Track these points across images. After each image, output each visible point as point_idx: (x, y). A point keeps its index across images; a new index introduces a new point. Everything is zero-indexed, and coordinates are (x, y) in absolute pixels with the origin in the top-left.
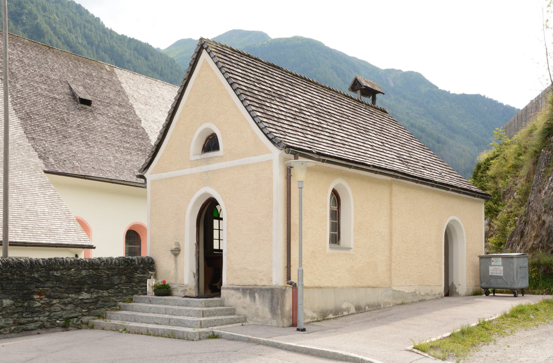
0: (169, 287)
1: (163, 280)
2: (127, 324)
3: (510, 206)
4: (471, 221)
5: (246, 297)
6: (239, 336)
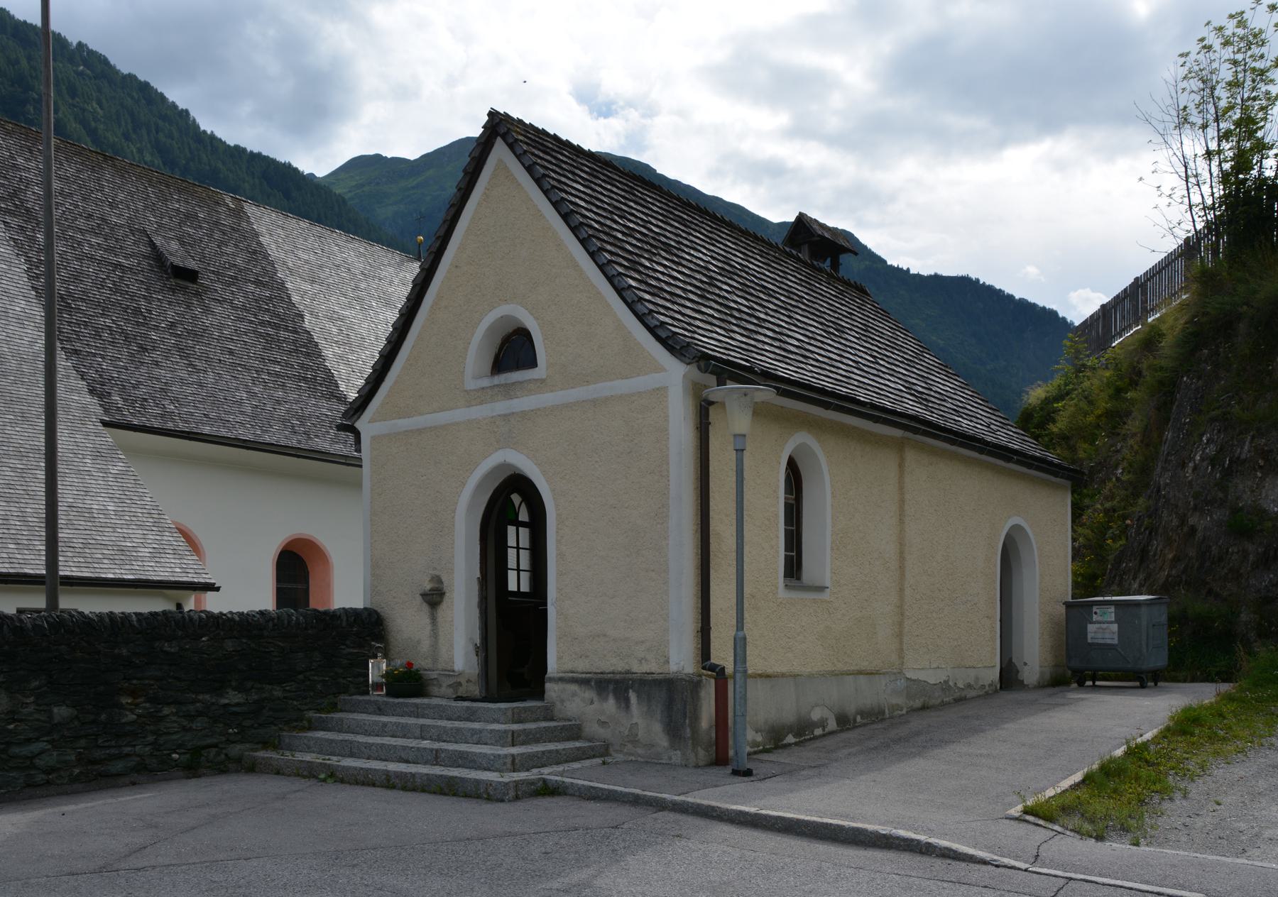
1: (405, 661)
2: (334, 760)
3: (1111, 497)
4: (1047, 525)
5: (606, 699)
6: (610, 791)
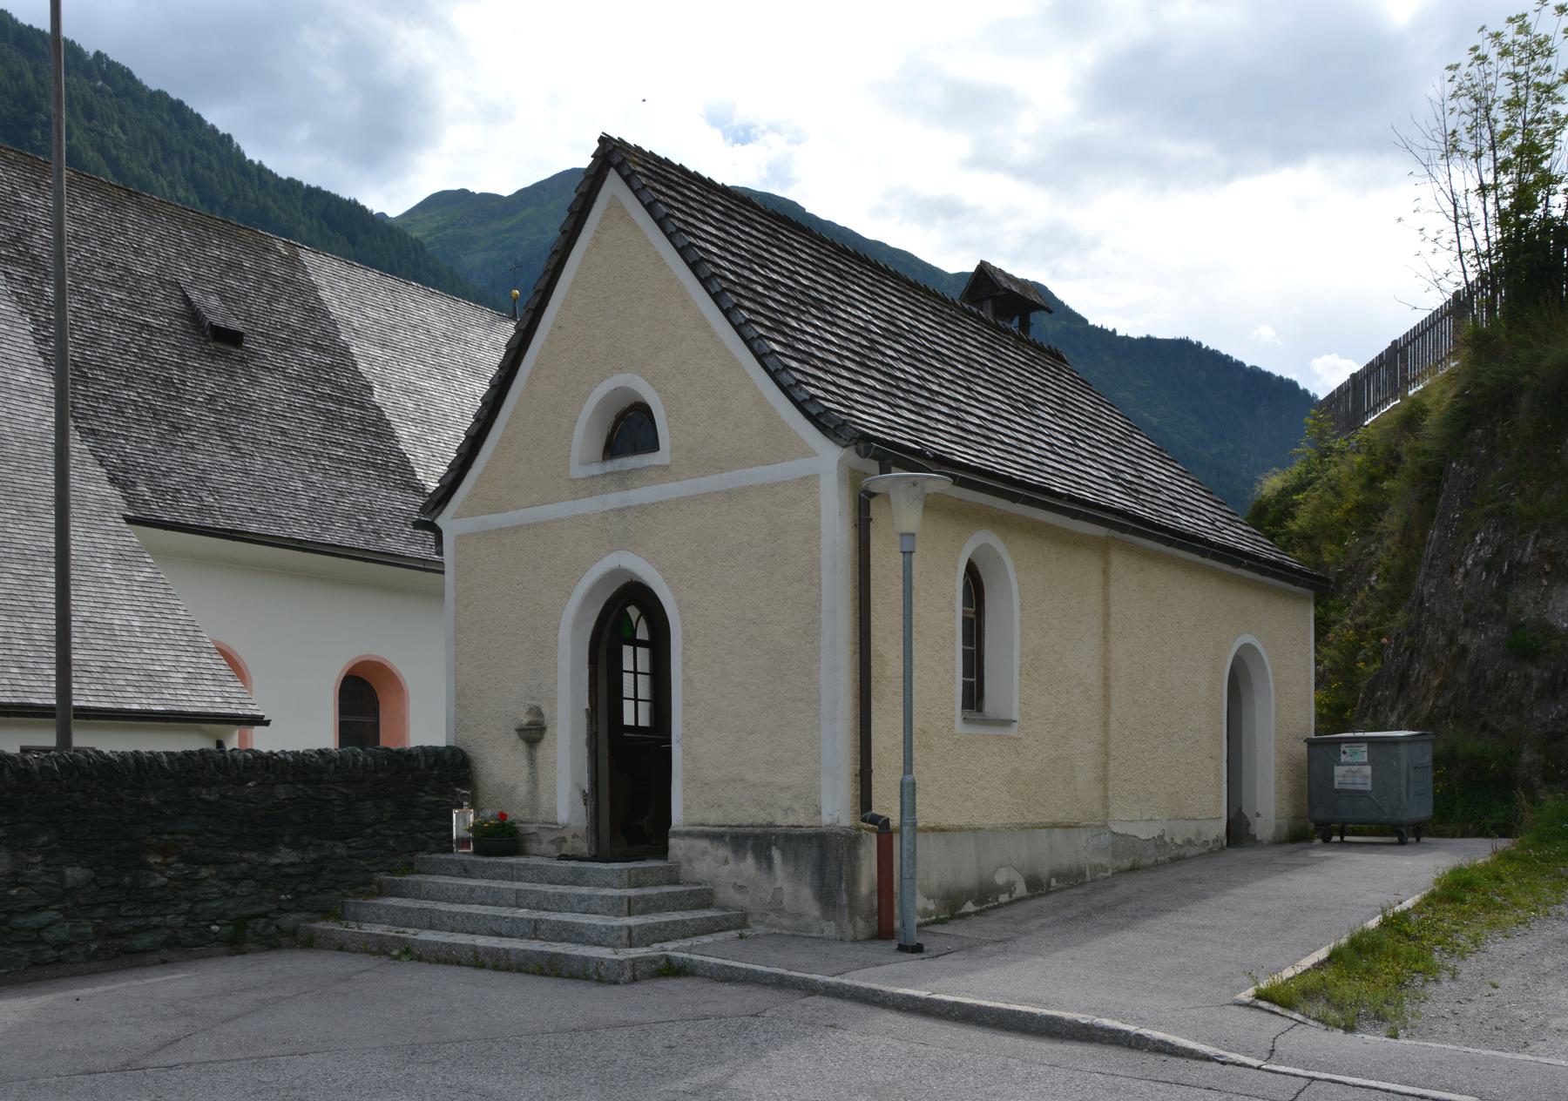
0: (516, 830)
1: (497, 811)
2: (410, 933)
3: (1363, 611)
4: (1285, 645)
5: (744, 858)
6: (748, 971)
